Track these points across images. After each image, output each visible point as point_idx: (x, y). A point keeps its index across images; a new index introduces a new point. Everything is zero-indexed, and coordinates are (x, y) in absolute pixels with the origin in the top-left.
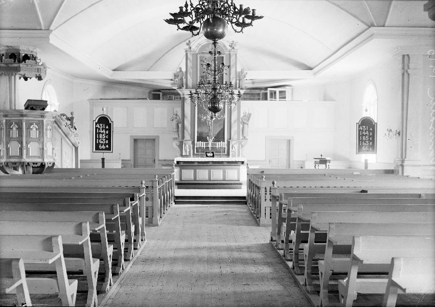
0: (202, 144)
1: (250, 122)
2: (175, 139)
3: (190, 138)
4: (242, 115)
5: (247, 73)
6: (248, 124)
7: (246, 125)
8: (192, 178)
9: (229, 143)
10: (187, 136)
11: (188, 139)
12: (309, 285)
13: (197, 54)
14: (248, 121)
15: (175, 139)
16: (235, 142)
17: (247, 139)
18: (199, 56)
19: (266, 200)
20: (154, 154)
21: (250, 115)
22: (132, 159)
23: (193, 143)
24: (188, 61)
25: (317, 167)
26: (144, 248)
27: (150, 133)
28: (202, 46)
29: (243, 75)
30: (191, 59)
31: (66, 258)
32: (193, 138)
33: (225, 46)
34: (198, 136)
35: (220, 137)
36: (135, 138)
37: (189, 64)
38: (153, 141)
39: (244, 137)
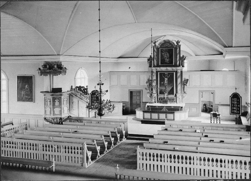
0: (162, 96)
1: (188, 84)
2: (148, 93)
3: (155, 92)
4: (183, 80)
5: (185, 58)
6: (186, 85)
7: (185, 86)
8: (157, 118)
9: (176, 96)
10: (154, 91)
11: (155, 93)
12: (117, 169)
13: (159, 48)
14: (187, 83)
15: (148, 93)
16: (179, 95)
17: (186, 93)
18: (160, 49)
19: (167, 161)
20: (140, 99)
21: (188, 80)
22: (130, 102)
23: (158, 94)
24: (155, 52)
25: (212, 121)
26: (64, 44)
27: (138, 89)
28: (162, 44)
29: (183, 59)
30: (156, 51)
31: (105, 137)
32: (157, 92)
33: (174, 43)
34: (160, 91)
35: (171, 92)
36: (131, 91)
37: (155, 54)
38: (139, 92)
39: (185, 92)
